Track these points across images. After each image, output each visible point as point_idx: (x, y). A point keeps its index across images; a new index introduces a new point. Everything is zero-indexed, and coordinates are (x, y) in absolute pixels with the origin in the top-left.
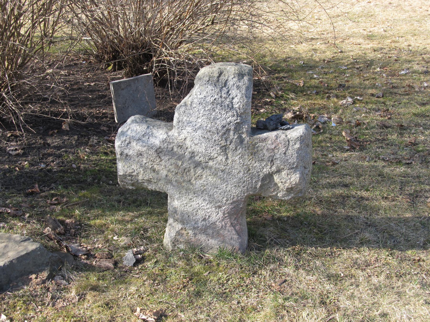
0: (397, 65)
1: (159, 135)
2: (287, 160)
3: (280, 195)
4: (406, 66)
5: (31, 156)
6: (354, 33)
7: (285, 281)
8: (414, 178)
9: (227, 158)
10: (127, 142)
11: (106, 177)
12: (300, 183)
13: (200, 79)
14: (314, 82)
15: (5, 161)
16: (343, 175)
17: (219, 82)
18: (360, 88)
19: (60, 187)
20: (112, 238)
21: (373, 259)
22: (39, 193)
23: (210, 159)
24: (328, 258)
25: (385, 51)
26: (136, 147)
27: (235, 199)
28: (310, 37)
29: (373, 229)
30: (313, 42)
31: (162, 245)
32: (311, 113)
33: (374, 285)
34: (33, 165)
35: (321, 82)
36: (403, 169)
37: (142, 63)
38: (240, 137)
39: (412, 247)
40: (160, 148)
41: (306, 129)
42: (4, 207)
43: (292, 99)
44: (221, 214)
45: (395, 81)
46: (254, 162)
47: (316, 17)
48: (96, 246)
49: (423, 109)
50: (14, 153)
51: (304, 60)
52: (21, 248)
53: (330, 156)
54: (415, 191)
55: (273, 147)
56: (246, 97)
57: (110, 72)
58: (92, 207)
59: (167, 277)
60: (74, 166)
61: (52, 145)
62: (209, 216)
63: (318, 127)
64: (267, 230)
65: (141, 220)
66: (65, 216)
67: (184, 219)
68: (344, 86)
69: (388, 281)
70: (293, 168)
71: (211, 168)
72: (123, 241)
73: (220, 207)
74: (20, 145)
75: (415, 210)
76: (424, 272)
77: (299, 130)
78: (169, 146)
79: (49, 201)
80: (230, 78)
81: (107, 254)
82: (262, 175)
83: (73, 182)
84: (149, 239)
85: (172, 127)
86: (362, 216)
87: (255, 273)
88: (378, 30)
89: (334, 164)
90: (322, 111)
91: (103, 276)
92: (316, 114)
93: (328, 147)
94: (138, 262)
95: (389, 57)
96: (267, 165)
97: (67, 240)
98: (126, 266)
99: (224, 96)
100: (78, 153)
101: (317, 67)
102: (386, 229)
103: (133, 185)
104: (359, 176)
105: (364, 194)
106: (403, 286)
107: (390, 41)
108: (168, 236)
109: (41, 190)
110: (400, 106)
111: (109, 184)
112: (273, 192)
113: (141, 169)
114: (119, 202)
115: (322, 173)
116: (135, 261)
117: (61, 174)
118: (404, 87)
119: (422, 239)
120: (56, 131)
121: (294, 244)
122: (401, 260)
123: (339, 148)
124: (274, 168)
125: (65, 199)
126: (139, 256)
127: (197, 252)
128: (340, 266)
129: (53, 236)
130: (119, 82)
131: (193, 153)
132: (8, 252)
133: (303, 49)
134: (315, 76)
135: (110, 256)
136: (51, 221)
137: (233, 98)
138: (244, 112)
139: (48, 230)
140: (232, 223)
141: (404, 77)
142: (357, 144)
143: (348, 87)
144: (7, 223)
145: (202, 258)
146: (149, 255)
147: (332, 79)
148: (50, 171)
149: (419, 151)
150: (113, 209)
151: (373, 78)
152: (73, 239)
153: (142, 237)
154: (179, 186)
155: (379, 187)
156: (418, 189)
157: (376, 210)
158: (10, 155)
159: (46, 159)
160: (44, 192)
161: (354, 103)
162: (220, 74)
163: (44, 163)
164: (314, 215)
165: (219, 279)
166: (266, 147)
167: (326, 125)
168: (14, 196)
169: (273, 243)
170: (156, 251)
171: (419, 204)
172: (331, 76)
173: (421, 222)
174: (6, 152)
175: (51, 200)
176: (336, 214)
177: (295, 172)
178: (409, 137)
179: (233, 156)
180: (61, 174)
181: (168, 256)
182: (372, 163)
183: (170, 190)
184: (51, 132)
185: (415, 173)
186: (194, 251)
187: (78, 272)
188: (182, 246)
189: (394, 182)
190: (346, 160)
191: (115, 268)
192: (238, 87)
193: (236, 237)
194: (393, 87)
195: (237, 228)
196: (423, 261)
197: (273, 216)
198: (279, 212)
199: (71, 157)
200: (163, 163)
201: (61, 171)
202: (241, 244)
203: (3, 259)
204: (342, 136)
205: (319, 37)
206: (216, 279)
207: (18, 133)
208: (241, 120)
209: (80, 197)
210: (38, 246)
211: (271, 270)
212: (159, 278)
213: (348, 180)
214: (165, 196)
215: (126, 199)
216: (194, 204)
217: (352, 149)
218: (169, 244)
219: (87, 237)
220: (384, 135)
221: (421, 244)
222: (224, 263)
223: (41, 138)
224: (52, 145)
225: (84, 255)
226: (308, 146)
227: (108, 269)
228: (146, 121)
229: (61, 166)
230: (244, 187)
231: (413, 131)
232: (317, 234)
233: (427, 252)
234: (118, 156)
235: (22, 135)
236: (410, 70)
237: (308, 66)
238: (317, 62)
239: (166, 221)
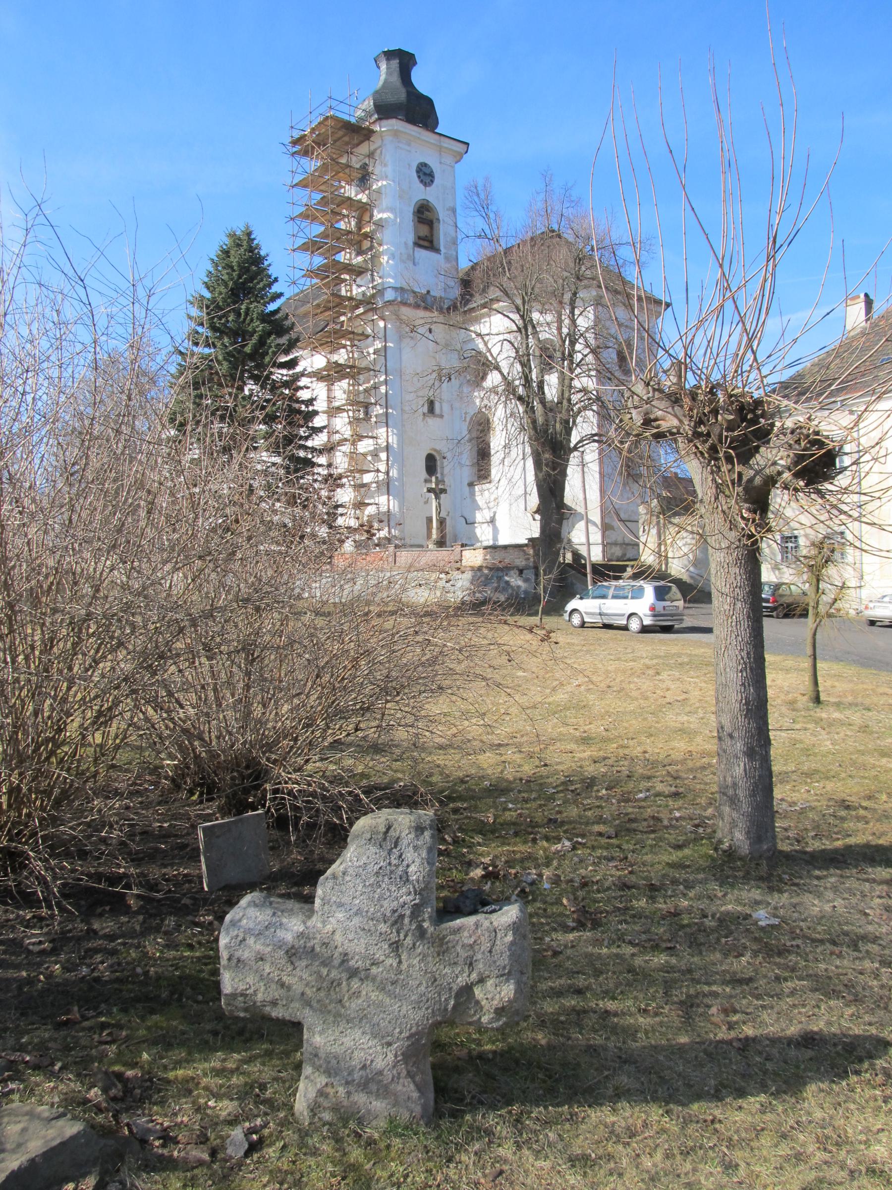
0: (631, 785)
1: (293, 926)
2: (495, 962)
3: (485, 1019)
4: (644, 784)
5: (66, 953)
6: (560, 733)
7: (501, 1172)
8: (683, 973)
9: (400, 962)
10: (239, 939)
11: (193, 988)
12: (516, 999)
13: (357, 836)
14: (509, 816)
15: (20, 963)
16: (572, 974)
17: (386, 839)
18: (581, 824)
19: (115, 1010)
20: (206, 1103)
21: (639, 1123)
22: (80, 1022)
23: (373, 964)
24: (567, 1126)
25: (610, 762)
26: (255, 945)
27: (414, 1030)
28: (496, 742)
29: (632, 1068)
30: (502, 750)
31: (293, 1115)
32: (510, 867)
33: (648, 1172)
34: (69, 970)
35: (520, 815)
36: (662, 959)
37: (247, 791)
38: (420, 927)
39: (699, 1097)
40: (293, 947)
41: (521, 910)
42: (18, 1050)
43: (479, 844)
44: (391, 1057)
45: (630, 810)
46: (442, 967)
47: (503, 711)
48: (179, 1119)
49: (680, 854)
50: (36, 949)
51: (491, 780)
52: (51, 1132)
53: (547, 939)
54: (689, 996)
55: (471, 941)
56: (428, 863)
57: (195, 803)
58: (169, 1046)
59: (302, 1176)
60: (139, 970)
61: (100, 933)
62: (372, 1061)
63: (523, 891)
64: (465, 1079)
65: (255, 1068)
66: (125, 1064)
67: (332, 1067)
68: (556, 821)
69: (668, 1163)
70: (505, 976)
71: (374, 979)
72: (226, 1108)
73: (389, 1044)
74: (46, 934)
75: (693, 1030)
76: (724, 1143)
77: (511, 913)
78: (308, 945)
79: (96, 1037)
80: (403, 835)
81: (198, 1136)
82: (455, 987)
83: (137, 1000)
84: (269, 1102)
85: (312, 912)
86: (611, 1045)
87: (450, 1160)
88: (597, 728)
89: (556, 954)
90: (527, 864)
91: (192, 1178)
92: (518, 868)
93: (542, 924)
94: (253, 1147)
95: (618, 772)
96: (463, 970)
97: (127, 1110)
98: (231, 1158)
99: (394, 862)
100: (145, 947)
101: (512, 790)
102: (653, 1068)
103: (246, 1010)
104: (598, 973)
105: (611, 1005)
106: (695, 1170)
107: (615, 745)
108: (303, 1099)
109: (82, 1016)
110: (644, 851)
111: (198, 1002)
112: (474, 1015)
113: (262, 984)
114: (215, 1033)
115: (539, 970)
116: (247, 1146)
117: (116, 986)
118: (645, 820)
119: (713, 1082)
120: (107, 908)
121: (509, 1103)
122: (684, 1122)
123: (560, 925)
124: (474, 976)
125: (124, 1033)
126: (254, 1136)
127: (352, 1125)
128: (587, 1138)
129: (104, 1105)
130: (213, 826)
131: (346, 954)
132: (27, 1141)
133: (488, 761)
134: (510, 806)
135: (203, 1139)
136: (99, 1076)
137: (408, 866)
138: (426, 887)
139: (95, 1094)
140: (408, 1072)
141: (643, 804)
142: (587, 919)
143: (563, 823)
144: (22, 1081)
145: (360, 1136)
146: (271, 1134)
147: (536, 809)
148: (97, 980)
149: (683, 927)
150: (206, 1048)
151: (598, 807)
152: (138, 1108)
153: (258, 1100)
154: (323, 1010)
155: (632, 992)
156: (692, 991)
157: (632, 1032)
158: (30, 952)
159: (91, 958)
160: (87, 1019)
161: (574, 848)
162: (389, 828)
163: (88, 966)
164: (535, 1046)
165: (392, 1175)
166: (460, 943)
167: (534, 888)
168: (36, 1029)
169: (475, 1102)
170: (284, 1124)
171: (697, 1019)
172: (534, 805)
173: (705, 1051)
174: (22, 946)
175: (100, 1034)
176: (570, 1042)
177: (507, 980)
178: (665, 903)
179: (409, 958)
180: (116, 986)
181: (304, 1134)
182: (614, 950)
183: (308, 1017)
184: (99, 910)
185: (683, 965)
186: (345, 1123)
187: (148, 1173)
188: (327, 1116)
189: (653, 983)
190: (573, 947)
191: (212, 1162)
192: (416, 848)
193: (415, 1095)
194: (631, 821)
195: (418, 1078)
196: (720, 1121)
197: (470, 1052)
198: (479, 1043)
199: (134, 955)
200: (298, 972)
201: (118, 980)
202: (424, 1107)
203: (18, 1156)
204: (562, 904)
205: (511, 741)
206: (385, 1174)
207: (44, 912)
208: (421, 900)
209: (148, 1029)
210: (82, 1128)
211: (476, 1154)
212: (289, 1178)
213: (581, 981)
214: (297, 1026)
215: (227, 1028)
216: (348, 1041)
217: (581, 926)
218: (305, 1113)
219: (162, 1103)
220: (626, 901)
221: (712, 1092)
222: (397, 1142)
223: (82, 921)
224: (100, 933)
225: (159, 1138)
226: (524, 937)
227: (201, 1163)
228: (271, 903)
229: (116, 971)
230: (427, 1009)
231: (669, 893)
232: (544, 1082)
233: (723, 1106)
234: (224, 962)
235: (52, 916)
236: (652, 792)
237: (499, 790)
238: (510, 782)
239: (298, 1067)
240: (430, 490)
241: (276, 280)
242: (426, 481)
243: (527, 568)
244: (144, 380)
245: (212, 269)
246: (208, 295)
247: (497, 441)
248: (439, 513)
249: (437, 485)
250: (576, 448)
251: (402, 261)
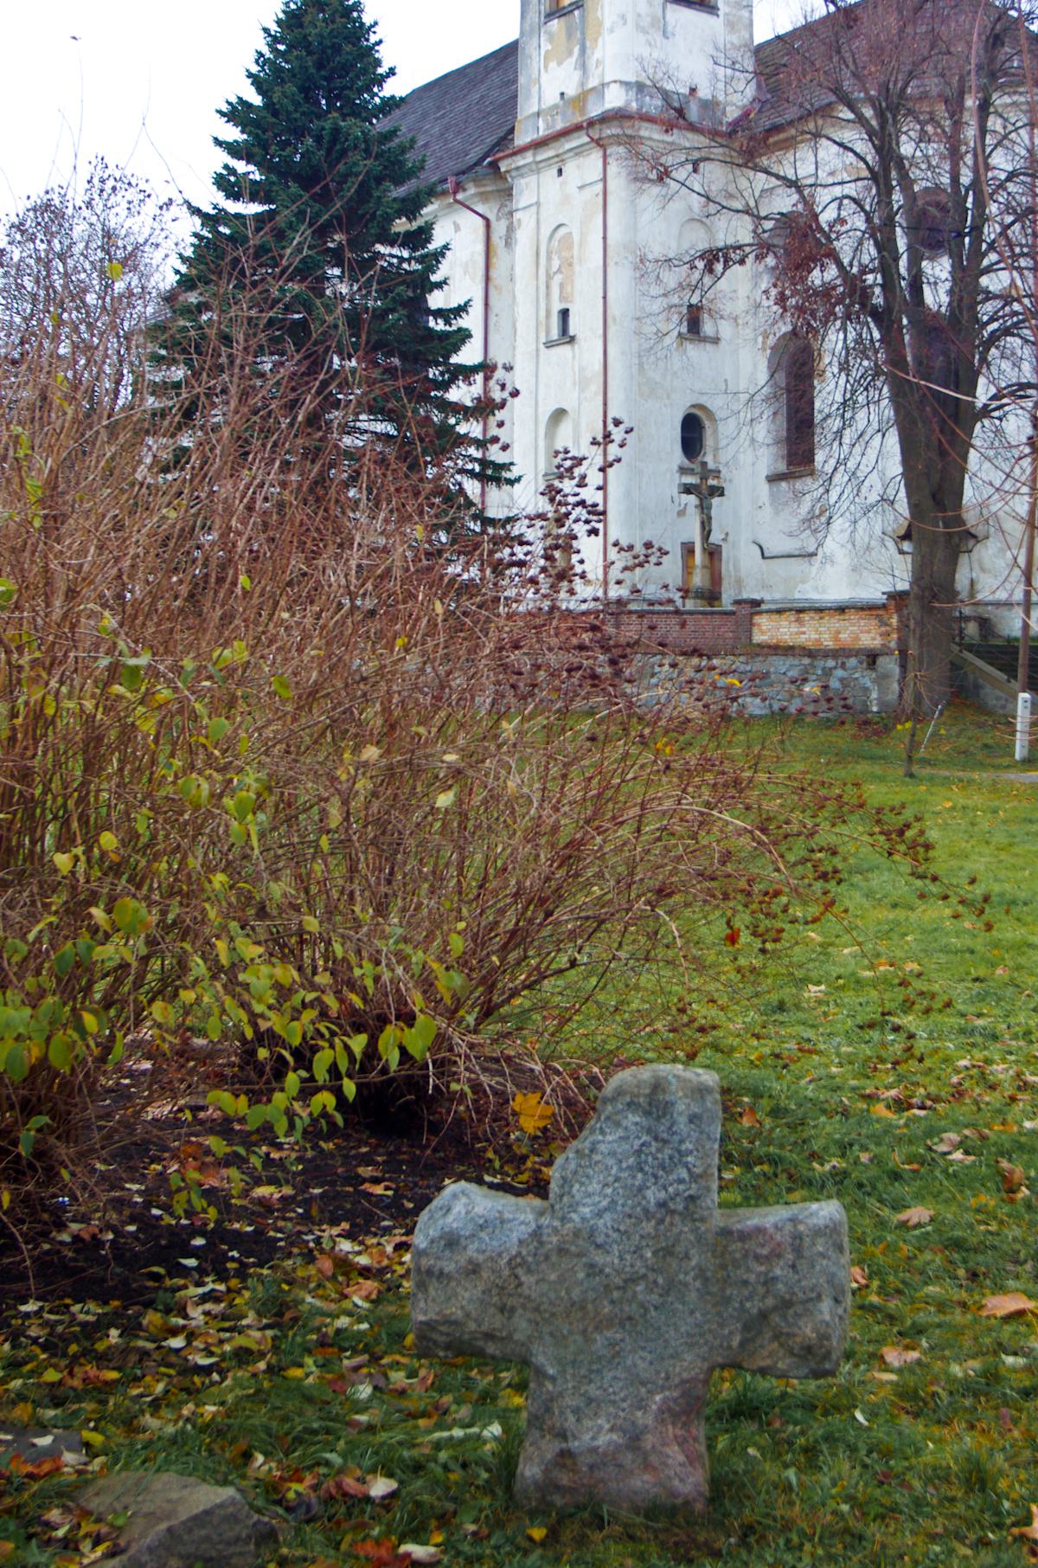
240: (687, 489)
241: (392, 72)
242: (683, 471)
243: (885, 651)
244: (934, 888)
245: (266, 51)
246: (256, 100)
247: (828, 392)
250: (986, 412)
251: (639, 28)
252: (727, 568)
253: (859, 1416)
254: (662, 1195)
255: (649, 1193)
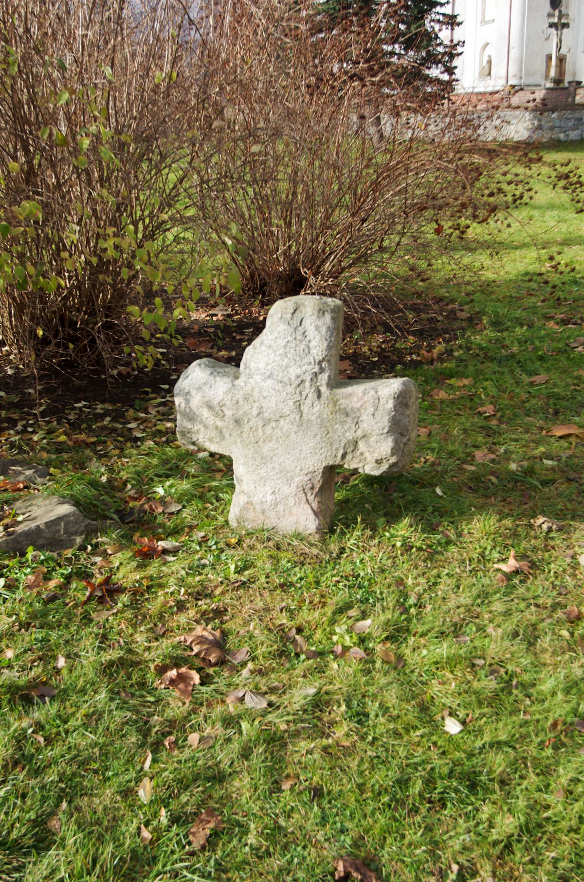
55: (358, 405)
99: (299, 337)
240: (551, 25)
242: (550, 15)
248: (559, 49)
249: (560, 18)
252: (568, 67)
253: (438, 491)
254: (298, 371)
255: (291, 370)
